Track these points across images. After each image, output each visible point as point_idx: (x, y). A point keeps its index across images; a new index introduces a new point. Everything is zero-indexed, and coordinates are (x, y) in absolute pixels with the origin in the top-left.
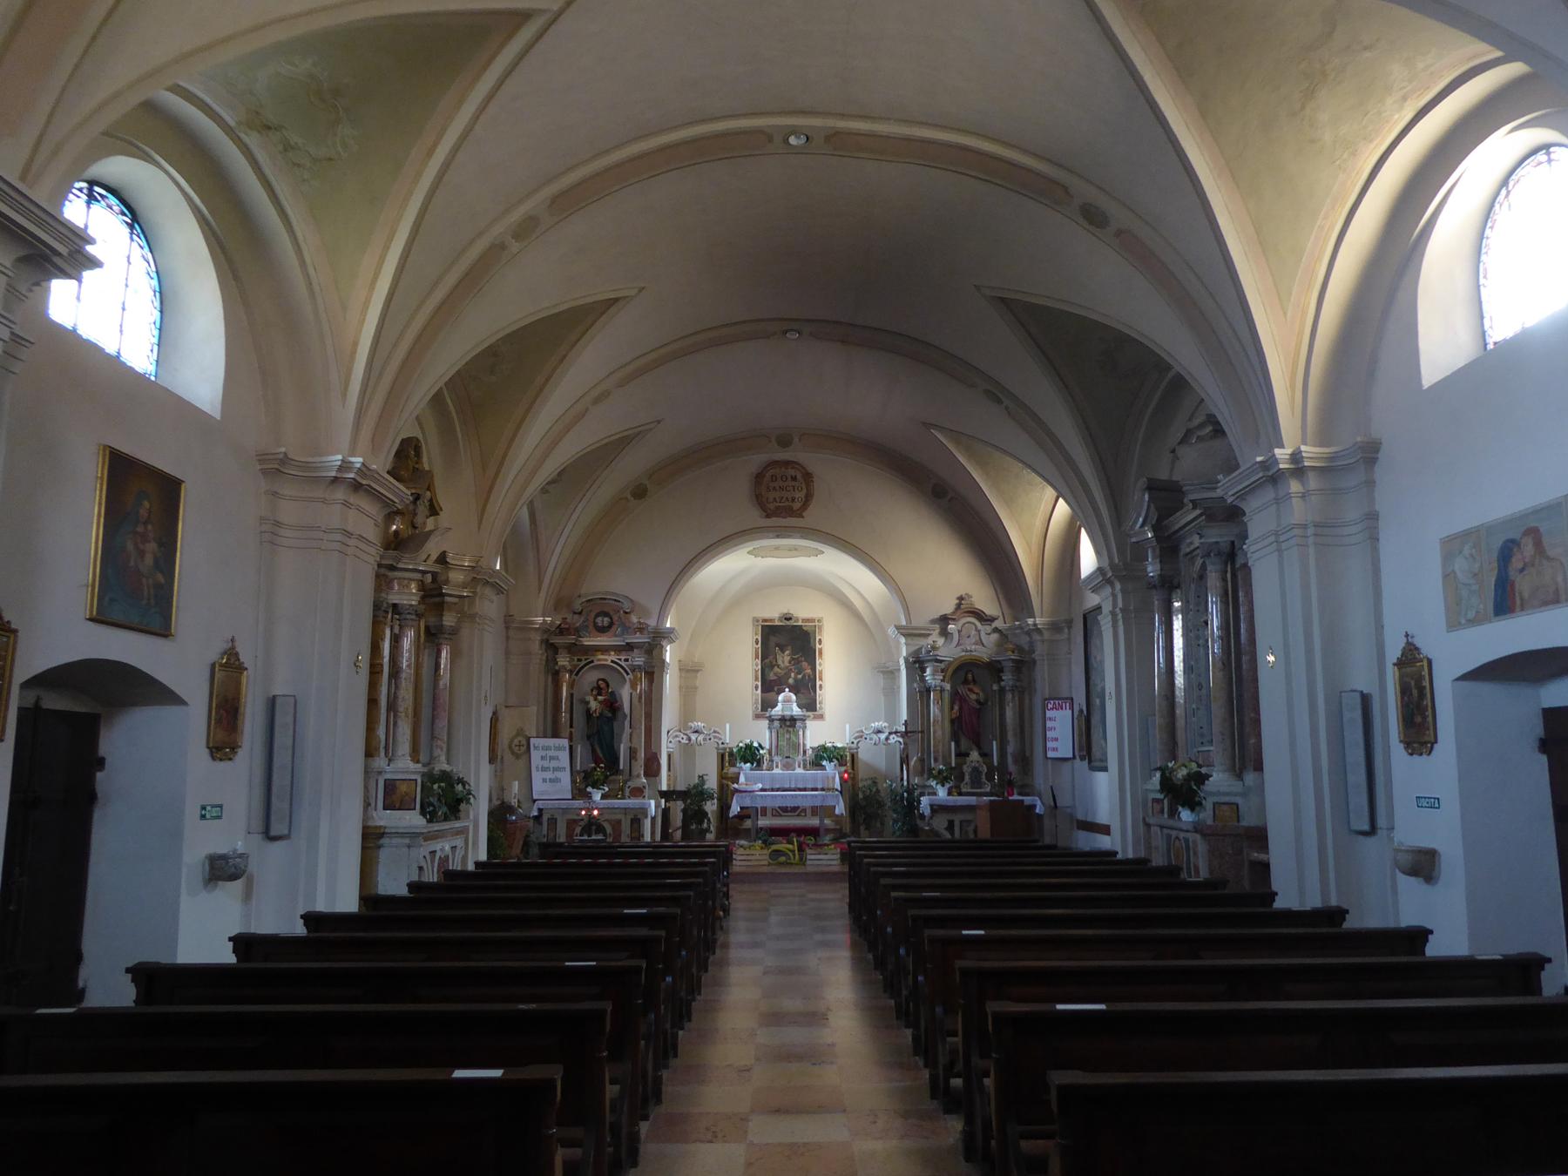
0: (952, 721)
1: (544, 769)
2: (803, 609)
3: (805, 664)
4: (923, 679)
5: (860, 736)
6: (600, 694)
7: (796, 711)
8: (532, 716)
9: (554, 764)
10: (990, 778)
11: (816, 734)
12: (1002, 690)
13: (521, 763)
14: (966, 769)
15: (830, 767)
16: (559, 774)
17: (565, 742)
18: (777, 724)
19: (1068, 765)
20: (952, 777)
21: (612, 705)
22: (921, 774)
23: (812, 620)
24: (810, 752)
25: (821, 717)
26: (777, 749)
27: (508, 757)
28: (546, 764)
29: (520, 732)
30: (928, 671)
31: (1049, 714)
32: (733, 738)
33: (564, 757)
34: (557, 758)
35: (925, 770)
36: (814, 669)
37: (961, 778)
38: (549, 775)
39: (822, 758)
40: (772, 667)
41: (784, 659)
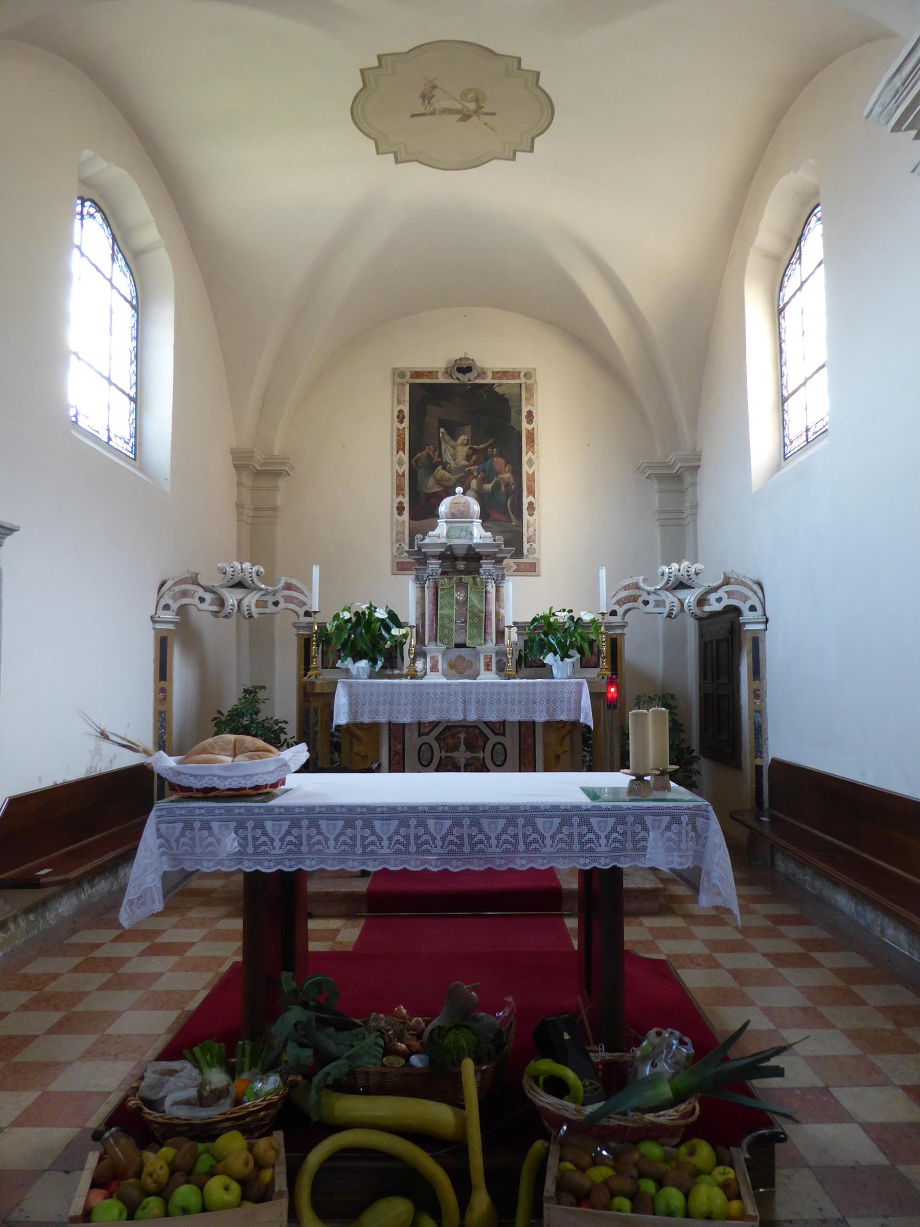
2: (498, 349)
3: (499, 462)
4: (571, 1161)
5: (632, 597)
7: (479, 534)
11: (520, 600)
18: (434, 565)
23: (515, 374)
24: (512, 636)
25: (532, 569)
26: (433, 627)
32: (323, 599)
36: (517, 472)
39: (545, 648)
40: (432, 467)
41: (456, 451)
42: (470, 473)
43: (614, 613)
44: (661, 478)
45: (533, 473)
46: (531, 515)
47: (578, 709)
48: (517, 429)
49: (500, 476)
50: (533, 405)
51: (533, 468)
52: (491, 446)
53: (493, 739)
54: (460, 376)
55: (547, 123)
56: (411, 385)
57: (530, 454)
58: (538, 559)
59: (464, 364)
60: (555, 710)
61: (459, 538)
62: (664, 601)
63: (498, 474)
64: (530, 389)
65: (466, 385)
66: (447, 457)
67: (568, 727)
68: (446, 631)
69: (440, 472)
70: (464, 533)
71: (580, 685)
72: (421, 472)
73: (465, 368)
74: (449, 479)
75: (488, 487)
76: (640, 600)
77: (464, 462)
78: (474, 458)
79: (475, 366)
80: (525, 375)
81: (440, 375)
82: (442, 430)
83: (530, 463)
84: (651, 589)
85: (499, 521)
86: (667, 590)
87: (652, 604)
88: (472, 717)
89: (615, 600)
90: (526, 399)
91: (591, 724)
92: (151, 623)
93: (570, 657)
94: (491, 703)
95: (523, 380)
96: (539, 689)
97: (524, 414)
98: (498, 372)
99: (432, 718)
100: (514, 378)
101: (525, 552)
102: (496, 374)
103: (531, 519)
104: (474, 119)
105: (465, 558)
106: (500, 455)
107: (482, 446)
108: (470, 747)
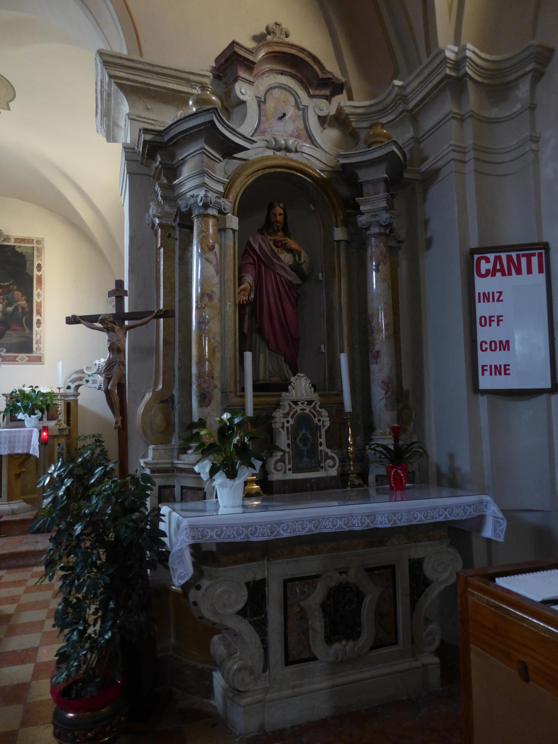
0: (241, 307)
3: (18, 294)
4: (171, 194)
10: (336, 440)
12: (358, 242)
14: (281, 420)
15: (31, 423)
19: (525, 410)
20: (240, 449)
22: (163, 436)
23: (30, 241)
30: (186, 171)
31: (482, 285)
35: (176, 426)
37: (270, 446)
43: (69, 387)
45: (41, 302)
46: (38, 327)
47: (29, 446)
48: (30, 274)
49: (19, 303)
50: (41, 260)
51: (41, 299)
55: (13, 93)
57: (39, 290)
58: (43, 354)
60: (14, 447)
62: (96, 380)
63: (17, 301)
64: (40, 251)
67: (23, 457)
73: (429, 243)
75: (10, 309)
76: (84, 380)
80: (37, 242)
83: (39, 295)
84: (89, 373)
85: (17, 330)
86: (98, 374)
87: (90, 382)
89: (70, 379)
90: (37, 256)
91: (38, 456)
92: (10, 393)
93: (35, 414)
95: (35, 245)
96: (3, 435)
98: (18, 239)
100: (29, 243)
101: (34, 350)
102: (17, 240)
103: (39, 330)
106: (19, 290)
107: (6, 284)
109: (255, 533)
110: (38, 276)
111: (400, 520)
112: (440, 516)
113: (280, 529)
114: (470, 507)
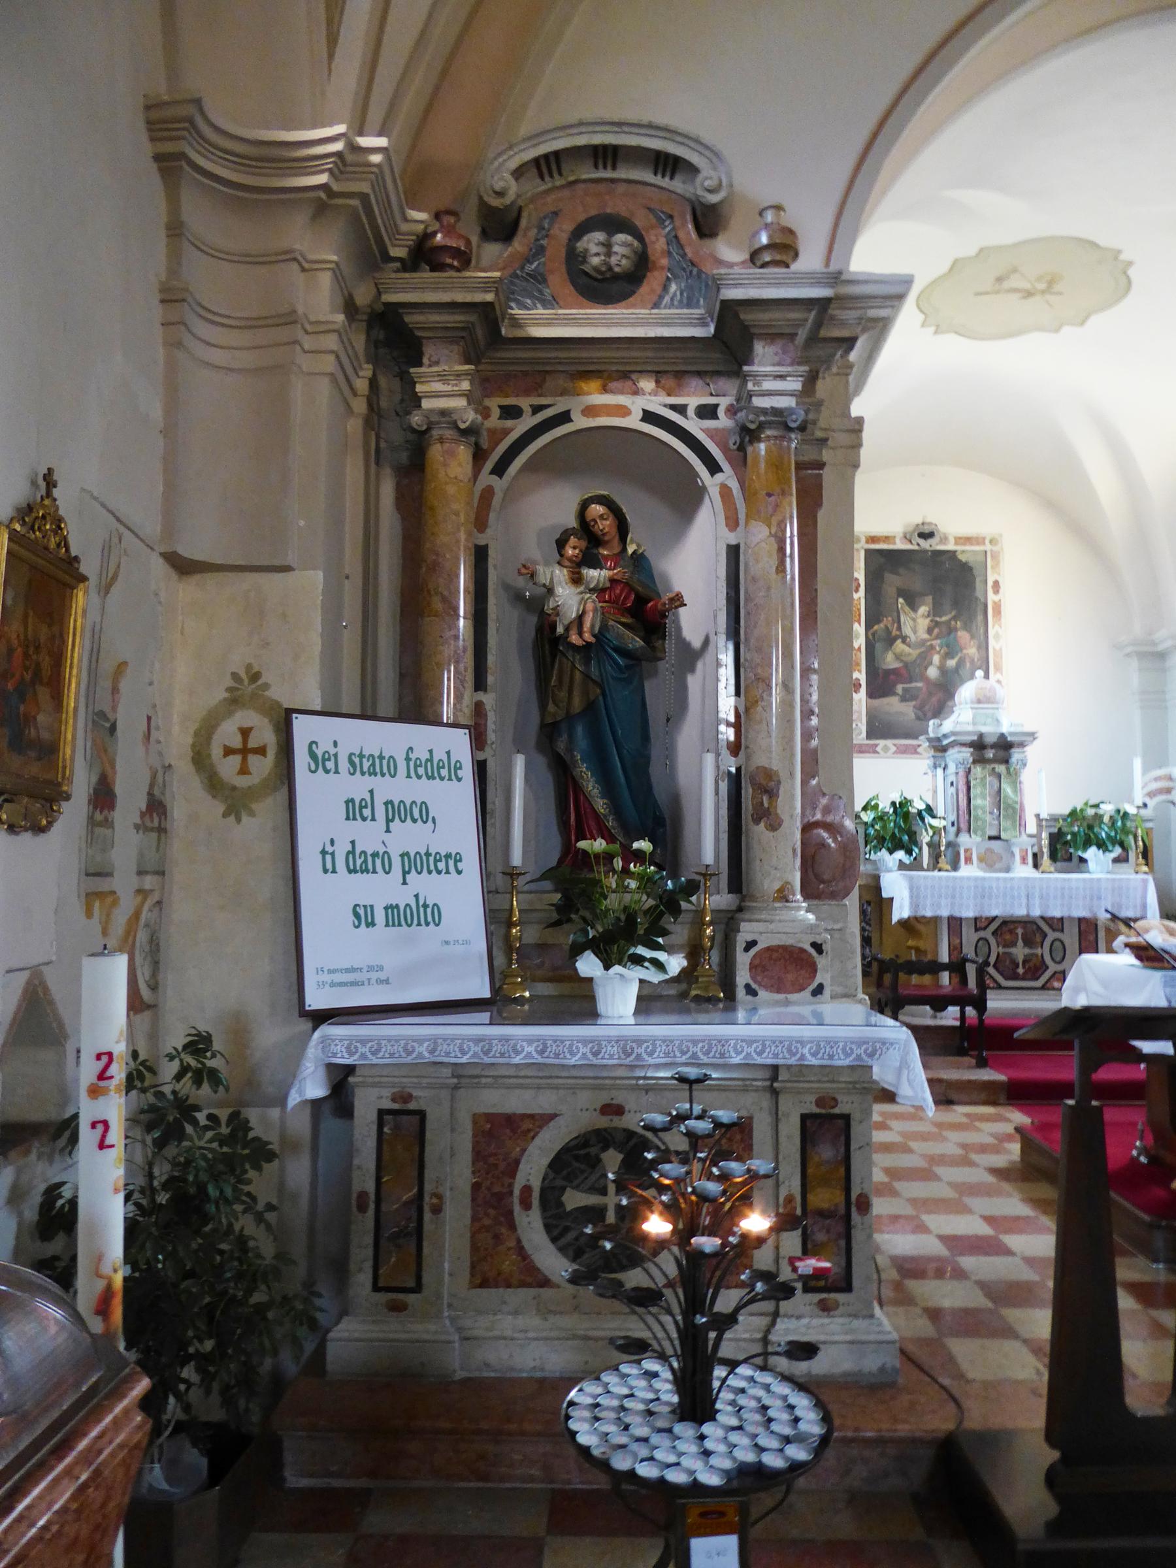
1: (362, 863)
6: (592, 561)
8: (301, 622)
9: (408, 837)
13: (256, 828)
16: (426, 886)
17: (458, 744)
21: (645, 610)
23: (979, 540)
27: (188, 800)
28: (369, 836)
29: (246, 689)
33: (455, 802)
34: (422, 814)
38: (381, 890)
40: (890, 641)
41: (916, 623)
42: (932, 647)
44: (1142, 655)
52: (955, 618)
53: (1051, 935)
54: (921, 541)
56: (868, 552)
59: (927, 529)
61: (985, 724)
64: (995, 556)
65: (926, 551)
66: (907, 630)
68: (980, 823)
69: (899, 646)
70: (989, 721)
71: (1145, 882)
72: (879, 646)
74: (910, 654)
77: (926, 636)
78: (936, 631)
79: (938, 531)
80: (991, 542)
81: (898, 540)
82: (901, 600)
88: (1036, 912)
94: (1055, 897)
95: (988, 547)
97: (990, 583)
99: (994, 912)
100: (978, 544)
102: (958, 540)
104: (1037, 298)
105: (993, 746)
107: (944, 619)
108: (1028, 942)
109: (489, 1050)
110: (995, 603)
111: (486, 1053)
112: (464, 1053)
113: (806, 1051)
114: (640, 1046)
